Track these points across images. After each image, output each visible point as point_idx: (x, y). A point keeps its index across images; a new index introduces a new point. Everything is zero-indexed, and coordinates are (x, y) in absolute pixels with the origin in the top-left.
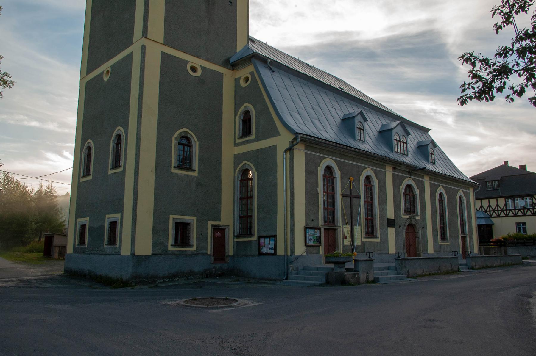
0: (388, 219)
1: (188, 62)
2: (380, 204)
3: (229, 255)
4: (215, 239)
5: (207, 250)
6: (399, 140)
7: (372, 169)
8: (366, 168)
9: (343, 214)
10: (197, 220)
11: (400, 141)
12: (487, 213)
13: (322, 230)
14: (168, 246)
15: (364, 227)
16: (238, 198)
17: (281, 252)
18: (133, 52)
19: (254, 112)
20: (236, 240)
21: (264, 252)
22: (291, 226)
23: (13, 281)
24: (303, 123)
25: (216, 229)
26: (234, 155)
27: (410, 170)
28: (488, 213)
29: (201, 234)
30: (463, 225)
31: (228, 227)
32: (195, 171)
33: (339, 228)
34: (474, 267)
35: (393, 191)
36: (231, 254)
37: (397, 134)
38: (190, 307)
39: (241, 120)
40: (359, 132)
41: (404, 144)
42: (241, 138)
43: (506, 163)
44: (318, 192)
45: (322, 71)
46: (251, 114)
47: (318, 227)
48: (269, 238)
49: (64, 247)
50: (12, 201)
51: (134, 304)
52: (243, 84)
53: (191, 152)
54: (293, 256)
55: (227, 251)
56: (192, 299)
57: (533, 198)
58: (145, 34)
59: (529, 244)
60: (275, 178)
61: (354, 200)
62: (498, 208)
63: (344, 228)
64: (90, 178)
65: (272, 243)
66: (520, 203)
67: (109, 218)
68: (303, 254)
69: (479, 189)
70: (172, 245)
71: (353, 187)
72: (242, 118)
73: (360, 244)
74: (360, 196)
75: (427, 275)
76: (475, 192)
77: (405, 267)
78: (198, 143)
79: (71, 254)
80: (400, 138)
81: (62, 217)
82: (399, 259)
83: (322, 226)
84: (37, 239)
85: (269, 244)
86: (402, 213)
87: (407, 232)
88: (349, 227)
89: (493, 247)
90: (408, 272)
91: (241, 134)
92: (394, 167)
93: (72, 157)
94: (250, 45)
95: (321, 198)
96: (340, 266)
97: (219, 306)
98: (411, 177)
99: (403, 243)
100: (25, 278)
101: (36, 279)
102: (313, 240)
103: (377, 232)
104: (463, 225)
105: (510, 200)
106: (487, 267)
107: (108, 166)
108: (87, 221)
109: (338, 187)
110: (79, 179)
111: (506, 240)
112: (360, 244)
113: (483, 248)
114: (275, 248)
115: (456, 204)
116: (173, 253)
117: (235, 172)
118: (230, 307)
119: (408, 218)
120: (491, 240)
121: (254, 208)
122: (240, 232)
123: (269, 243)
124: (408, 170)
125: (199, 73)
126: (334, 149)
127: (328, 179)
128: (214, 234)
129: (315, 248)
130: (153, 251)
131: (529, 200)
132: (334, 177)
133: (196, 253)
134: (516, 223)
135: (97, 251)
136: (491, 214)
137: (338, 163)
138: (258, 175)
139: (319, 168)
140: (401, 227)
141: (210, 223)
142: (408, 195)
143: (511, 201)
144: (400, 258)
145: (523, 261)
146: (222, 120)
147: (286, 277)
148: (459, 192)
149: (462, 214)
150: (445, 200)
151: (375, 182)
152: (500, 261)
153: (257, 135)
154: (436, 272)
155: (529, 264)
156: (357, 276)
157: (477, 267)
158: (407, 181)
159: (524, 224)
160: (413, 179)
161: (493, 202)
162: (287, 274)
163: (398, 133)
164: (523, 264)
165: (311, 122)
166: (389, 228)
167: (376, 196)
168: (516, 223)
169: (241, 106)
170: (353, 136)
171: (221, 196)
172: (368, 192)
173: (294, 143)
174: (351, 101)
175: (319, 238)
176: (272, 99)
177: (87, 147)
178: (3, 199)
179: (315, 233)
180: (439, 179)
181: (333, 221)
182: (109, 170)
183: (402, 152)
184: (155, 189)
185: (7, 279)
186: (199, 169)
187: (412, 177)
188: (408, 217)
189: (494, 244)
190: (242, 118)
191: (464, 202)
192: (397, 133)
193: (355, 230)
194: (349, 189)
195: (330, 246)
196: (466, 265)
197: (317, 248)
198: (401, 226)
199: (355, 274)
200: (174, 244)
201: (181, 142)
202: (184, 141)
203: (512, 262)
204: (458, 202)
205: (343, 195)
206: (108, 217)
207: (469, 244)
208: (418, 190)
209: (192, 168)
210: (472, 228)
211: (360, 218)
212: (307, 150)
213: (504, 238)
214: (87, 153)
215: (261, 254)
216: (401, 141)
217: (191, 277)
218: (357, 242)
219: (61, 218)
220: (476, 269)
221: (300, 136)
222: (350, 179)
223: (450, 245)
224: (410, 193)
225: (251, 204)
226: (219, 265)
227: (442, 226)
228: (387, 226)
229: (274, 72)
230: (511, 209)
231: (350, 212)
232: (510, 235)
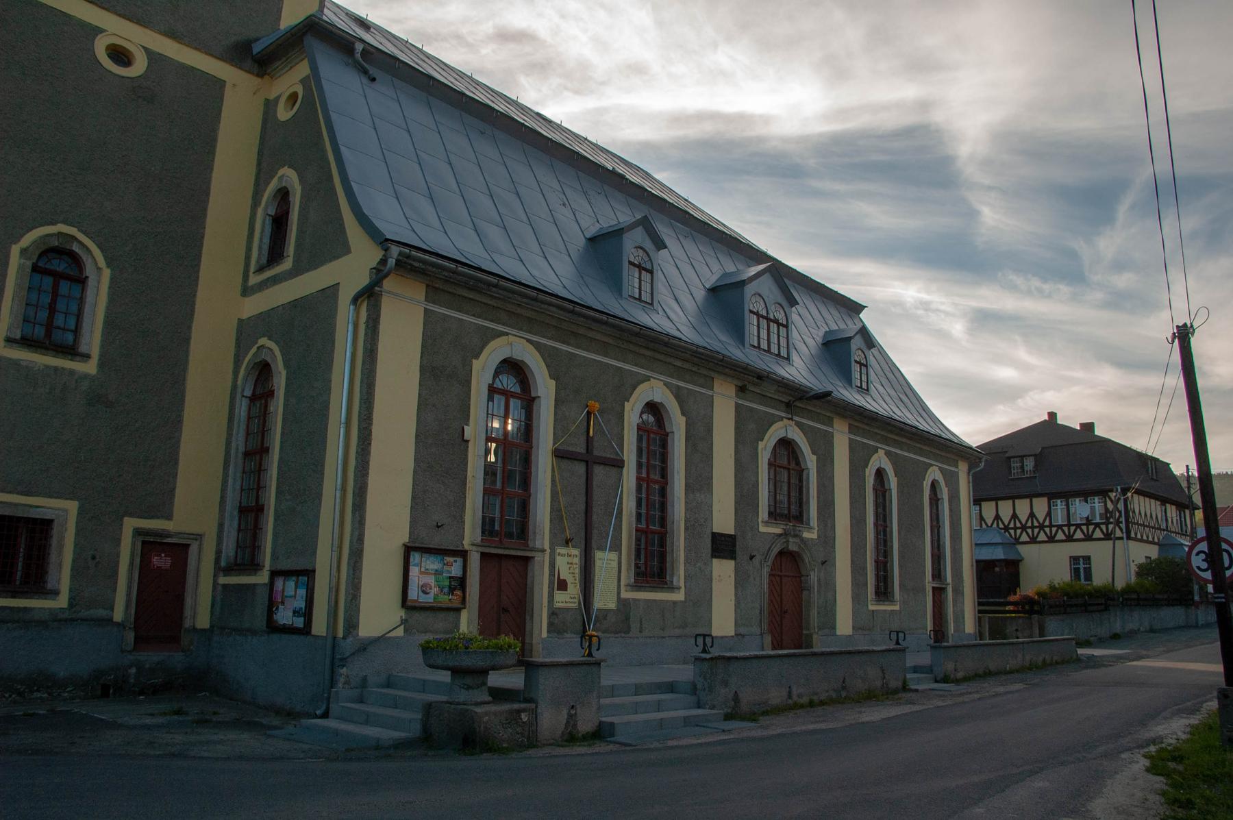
0: (714, 534)
1: (98, 31)
2: (688, 487)
3: (194, 626)
4: (146, 574)
6: (765, 314)
8: (647, 379)
10: (81, 512)
11: (767, 318)
12: (1010, 534)
13: (475, 560)
16: (237, 449)
20: (223, 580)
22: (351, 542)
24: (436, 223)
25: (150, 544)
26: (240, 321)
27: (791, 398)
28: (1013, 532)
29: (94, 558)
30: (938, 558)
31: (196, 540)
33: (540, 554)
34: (952, 676)
35: (735, 454)
36: (203, 621)
37: (758, 299)
39: (267, 217)
40: (637, 275)
41: (781, 327)
43: (1052, 415)
47: (460, 548)
51: (97, 736)
54: (350, 640)
55: (188, 612)
57: (1107, 499)
59: (1095, 608)
61: (599, 472)
62: (1032, 522)
63: (559, 554)
65: (302, 592)
66: (1081, 509)
68: (389, 635)
69: (983, 464)
72: (272, 211)
73: (612, 605)
74: (623, 461)
75: (802, 706)
76: (972, 472)
77: (726, 683)
78: (107, 273)
80: (767, 311)
82: (705, 659)
85: (295, 596)
86: (760, 520)
87: (773, 575)
89: (1014, 615)
90: (736, 698)
92: (740, 384)
96: (469, 680)
98: (792, 419)
99: (758, 606)
103: (675, 571)
104: (938, 558)
105: (1059, 501)
106: (988, 674)
111: (1044, 598)
112: (612, 605)
113: (987, 620)
115: (922, 504)
119: (781, 535)
120: (1012, 598)
122: (236, 557)
124: (785, 399)
125: (139, 66)
126: (532, 310)
127: (652, 435)
129: (442, 615)
131: (1099, 503)
132: (533, 395)
133: (66, 615)
134: (1070, 557)
136: (1018, 536)
138: (287, 379)
139: (476, 364)
140: (756, 561)
142: (784, 468)
143: (1061, 505)
144: (708, 656)
145: (1080, 651)
147: (324, 707)
148: (930, 470)
149: (936, 531)
150: (890, 489)
151: (678, 424)
152: (1023, 655)
153: (297, 260)
154: (834, 695)
155: (1092, 663)
156: (524, 717)
157: (960, 675)
158: (782, 428)
159: (1087, 559)
160: (798, 424)
161: (1023, 508)
162: (328, 699)
163: (762, 294)
164: (1078, 660)
166: (715, 561)
167: (676, 464)
168: (1070, 557)
170: (615, 283)
171: (179, 441)
172: (655, 452)
174: (630, 199)
175: (460, 583)
179: (446, 568)
180: (876, 431)
181: (523, 531)
183: (774, 349)
186: (102, 356)
187: (795, 418)
188: (778, 531)
189: (1016, 609)
190: (273, 214)
191: (944, 497)
192: (760, 295)
193: (598, 563)
194: (585, 437)
195: (505, 610)
196: (929, 670)
197: (452, 615)
198: (754, 556)
199: (519, 711)
202: (59, 265)
203: (1052, 658)
204: (928, 496)
205: (559, 454)
207: (953, 607)
208: (814, 458)
209: (78, 349)
210: (962, 566)
211: (618, 527)
213: (1039, 594)
215: (273, 628)
216: (772, 317)
217: (39, 695)
218: (605, 599)
220: (957, 681)
222: (587, 406)
223: (900, 612)
224: (789, 463)
226: (151, 657)
227: (881, 558)
228: (709, 555)
229: (373, 80)
230: (1060, 523)
231: (583, 507)
232: (1054, 585)
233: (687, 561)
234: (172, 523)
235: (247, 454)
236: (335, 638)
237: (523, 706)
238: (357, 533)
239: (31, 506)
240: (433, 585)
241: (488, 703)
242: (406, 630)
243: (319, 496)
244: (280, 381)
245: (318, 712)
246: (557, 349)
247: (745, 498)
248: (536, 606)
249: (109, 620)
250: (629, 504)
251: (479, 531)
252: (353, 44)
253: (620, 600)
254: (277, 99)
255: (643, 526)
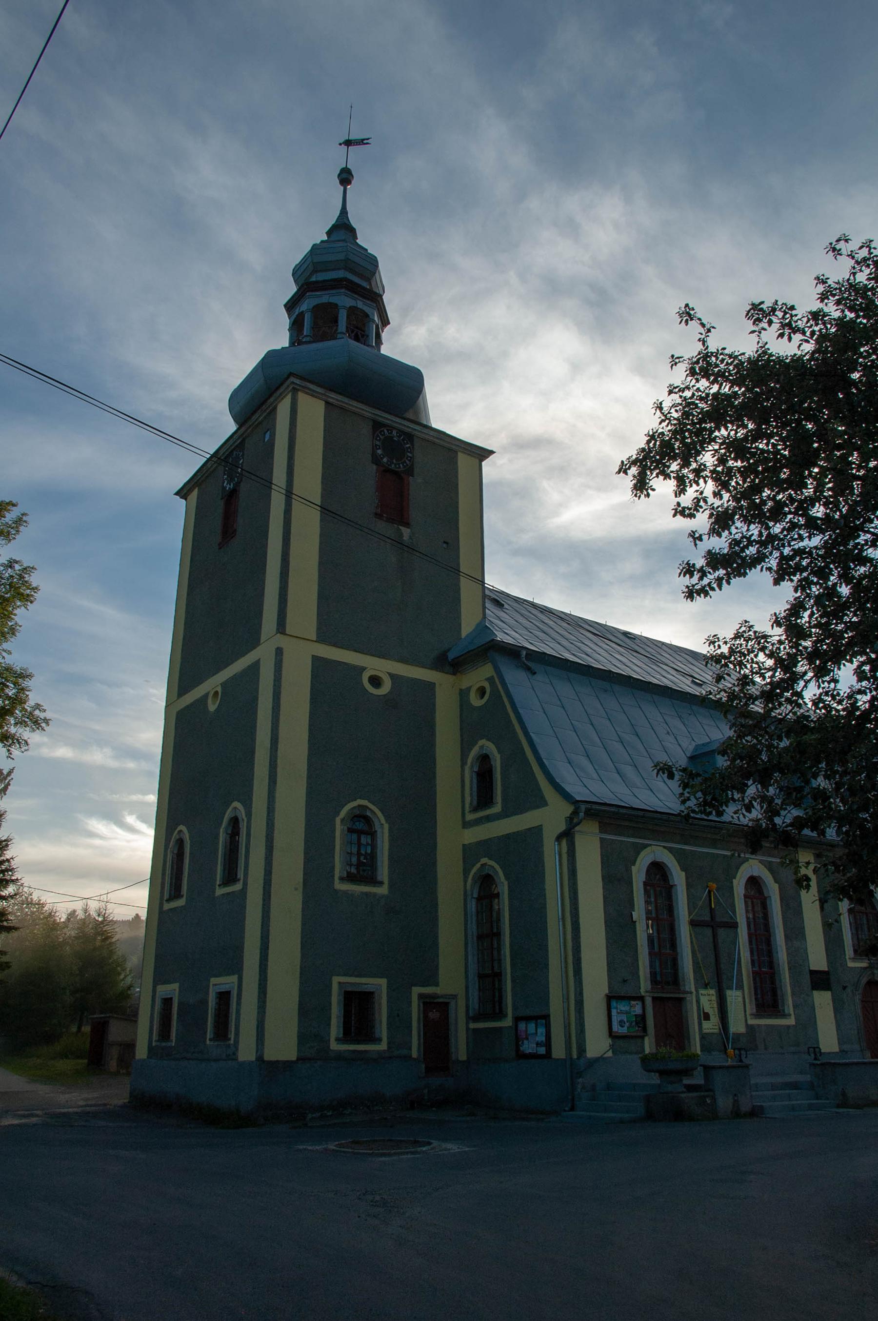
1: (363, 669)
2: (787, 937)
4: (426, 1022)
5: (410, 1049)
7: (761, 862)
9: (696, 963)
13: (649, 1001)
14: (329, 1040)
15: (750, 992)
17: (558, 1052)
18: (259, 659)
19: (498, 757)
20: (472, 1026)
21: (527, 1052)
22: (575, 994)
23: (37, 1116)
25: (429, 1003)
32: (381, 883)
36: (463, 1056)
38: (342, 1154)
42: (475, 810)
44: (634, 919)
45: (660, 645)
46: (492, 763)
48: (534, 1021)
49: (129, 1047)
50: (27, 943)
52: (476, 701)
53: (374, 846)
55: (453, 1050)
56: (352, 1142)
58: (281, 628)
60: (543, 891)
61: (722, 933)
64: (181, 902)
65: (542, 1030)
67: (216, 985)
70: (338, 1040)
71: (718, 903)
72: (476, 769)
73: (742, 1030)
74: (737, 923)
78: (386, 826)
79: (144, 1060)
81: (126, 976)
83: (647, 992)
84: (74, 1029)
85: (536, 1033)
86: (847, 957)
88: (714, 993)
90: (844, 1094)
91: (475, 803)
92: (817, 852)
93: (151, 832)
94: (491, 616)
95: (643, 931)
97: (392, 1152)
100: (58, 1110)
101: (77, 1113)
102: (627, 1024)
107: (216, 880)
108: (175, 990)
109: (680, 903)
110: (161, 905)
112: (742, 1030)
114: (548, 1044)
116: (339, 1057)
117: (465, 882)
118: (412, 1153)
119: (865, 968)
121: (505, 956)
123: (534, 1032)
125: (386, 687)
128: (426, 1017)
130: (299, 1051)
132: (671, 884)
135: (194, 1052)
137: (680, 856)
138: (509, 887)
139: (634, 869)
140: (849, 990)
141: (416, 990)
144: (819, 1062)
146: (434, 777)
147: (570, 1105)
156: (708, 1101)
162: (573, 1100)
165: (615, 771)
169: (474, 746)
173: (575, 820)
175: (641, 1020)
176: (529, 733)
177: (178, 840)
178: (11, 941)
181: (675, 980)
182: (217, 887)
184: (304, 924)
185: (26, 1113)
188: (864, 964)
193: (729, 999)
200: (342, 1035)
201: (354, 827)
202: (359, 826)
205: (693, 923)
206: (215, 983)
212: (606, 832)
214: (176, 852)
215: (522, 1056)
218: (737, 1026)
219: (123, 980)
221: (583, 807)
222: (708, 887)
225: (499, 950)
229: (535, 673)
233: (793, 994)
234: (438, 988)
235: (480, 937)
236: (571, 1058)
237: (706, 1093)
238: (578, 990)
239: (362, 984)
240: (625, 1020)
241: (685, 1092)
242: (613, 1052)
243: (546, 966)
244: (503, 887)
245: (567, 1109)
246: (684, 849)
247: (833, 942)
248: (691, 1033)
249: (410, 1057)
250: (745, 955)
251: (649, 982)
252: (520, 651)
253: (747, 1026)
254: (469, 689)
255: (756, 969)
